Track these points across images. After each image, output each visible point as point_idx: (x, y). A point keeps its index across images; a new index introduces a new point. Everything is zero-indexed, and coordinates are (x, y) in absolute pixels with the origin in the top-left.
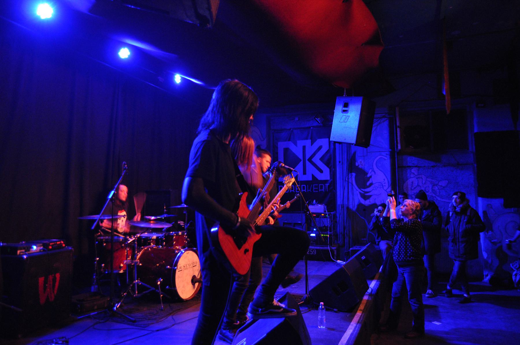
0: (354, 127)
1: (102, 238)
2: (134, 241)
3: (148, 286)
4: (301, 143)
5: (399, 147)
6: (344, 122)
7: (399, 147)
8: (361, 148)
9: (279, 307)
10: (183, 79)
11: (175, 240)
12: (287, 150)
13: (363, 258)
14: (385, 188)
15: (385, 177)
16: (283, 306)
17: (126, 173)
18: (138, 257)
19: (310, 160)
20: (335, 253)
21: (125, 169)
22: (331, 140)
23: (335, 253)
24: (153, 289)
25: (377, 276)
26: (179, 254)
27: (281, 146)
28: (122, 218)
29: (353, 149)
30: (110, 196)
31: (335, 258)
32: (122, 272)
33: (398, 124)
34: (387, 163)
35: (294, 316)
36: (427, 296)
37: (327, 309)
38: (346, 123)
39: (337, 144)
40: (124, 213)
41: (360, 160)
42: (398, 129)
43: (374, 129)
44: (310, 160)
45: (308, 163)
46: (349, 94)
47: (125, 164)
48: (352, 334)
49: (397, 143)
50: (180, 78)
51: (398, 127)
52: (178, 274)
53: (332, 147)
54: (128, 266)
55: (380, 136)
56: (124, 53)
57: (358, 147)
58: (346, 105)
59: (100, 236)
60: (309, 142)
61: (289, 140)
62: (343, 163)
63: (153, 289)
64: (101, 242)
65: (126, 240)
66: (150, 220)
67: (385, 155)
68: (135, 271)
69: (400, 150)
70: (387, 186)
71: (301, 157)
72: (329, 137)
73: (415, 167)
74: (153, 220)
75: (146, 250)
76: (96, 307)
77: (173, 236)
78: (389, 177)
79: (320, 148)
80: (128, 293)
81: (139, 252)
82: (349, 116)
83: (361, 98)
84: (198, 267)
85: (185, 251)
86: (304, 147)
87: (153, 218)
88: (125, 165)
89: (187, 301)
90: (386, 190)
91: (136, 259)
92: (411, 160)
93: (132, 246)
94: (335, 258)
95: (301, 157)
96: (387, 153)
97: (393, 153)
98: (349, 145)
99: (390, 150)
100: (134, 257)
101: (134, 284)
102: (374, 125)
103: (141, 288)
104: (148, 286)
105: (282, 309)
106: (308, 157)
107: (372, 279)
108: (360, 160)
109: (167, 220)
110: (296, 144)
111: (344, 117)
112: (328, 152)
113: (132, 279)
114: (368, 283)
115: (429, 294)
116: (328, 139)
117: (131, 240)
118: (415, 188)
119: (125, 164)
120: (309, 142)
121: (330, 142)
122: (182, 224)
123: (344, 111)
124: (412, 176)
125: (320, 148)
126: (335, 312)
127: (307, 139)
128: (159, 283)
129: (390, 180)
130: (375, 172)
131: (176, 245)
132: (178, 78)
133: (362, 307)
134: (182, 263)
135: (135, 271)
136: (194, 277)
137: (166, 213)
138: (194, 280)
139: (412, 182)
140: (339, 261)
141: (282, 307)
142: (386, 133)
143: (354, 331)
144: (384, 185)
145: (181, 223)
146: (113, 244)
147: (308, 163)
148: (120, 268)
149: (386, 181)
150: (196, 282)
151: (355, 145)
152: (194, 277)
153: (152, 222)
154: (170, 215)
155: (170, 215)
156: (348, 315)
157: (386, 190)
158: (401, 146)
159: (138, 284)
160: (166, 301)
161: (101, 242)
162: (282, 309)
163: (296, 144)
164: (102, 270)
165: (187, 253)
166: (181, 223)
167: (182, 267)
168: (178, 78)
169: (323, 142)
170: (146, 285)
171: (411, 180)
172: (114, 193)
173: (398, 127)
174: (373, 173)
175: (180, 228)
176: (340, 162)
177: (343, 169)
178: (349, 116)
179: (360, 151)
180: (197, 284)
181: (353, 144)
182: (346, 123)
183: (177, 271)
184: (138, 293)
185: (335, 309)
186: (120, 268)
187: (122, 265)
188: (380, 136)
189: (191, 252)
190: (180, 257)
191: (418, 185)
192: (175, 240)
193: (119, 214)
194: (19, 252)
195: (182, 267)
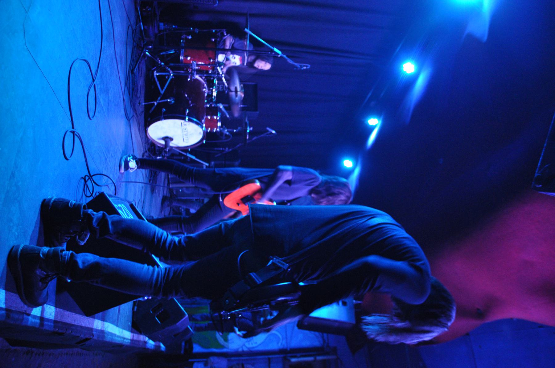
5: (294, 360)
11: (212, 118)
14: (247, 344)
15: (258, 343)
24: (162, 92)
30: (276, 50)
32: (181, 58)
33: (319, 358)
47: (307, 66)
51: (315, 358)
52: (178, 122)
54: (188, 65)
69: (289, 361)
75: (203, 85)
78: (261, 348)
84: (182, 144)
89: (146, 131)
96: (285, 346)
99: (288, 349)
100: (199, 72)
129: (256, 349)
136: (172, 139)
138: (167, 139)
142: (306, 344)
143: (118, 337)
144: (250, 343)
146: (209, 46)
148: (186, 56)
149: (254, 345)
150: (166, 142)
152: (172, 139)
160: (147, 108)
164: (184, 36)
165: (200, 133)
172: (278, 54)
180: (163, 142)
185: (136, 308)
187: (189, 58)
189: (200, 137)
192: (212, 118)
195: (185, 127)
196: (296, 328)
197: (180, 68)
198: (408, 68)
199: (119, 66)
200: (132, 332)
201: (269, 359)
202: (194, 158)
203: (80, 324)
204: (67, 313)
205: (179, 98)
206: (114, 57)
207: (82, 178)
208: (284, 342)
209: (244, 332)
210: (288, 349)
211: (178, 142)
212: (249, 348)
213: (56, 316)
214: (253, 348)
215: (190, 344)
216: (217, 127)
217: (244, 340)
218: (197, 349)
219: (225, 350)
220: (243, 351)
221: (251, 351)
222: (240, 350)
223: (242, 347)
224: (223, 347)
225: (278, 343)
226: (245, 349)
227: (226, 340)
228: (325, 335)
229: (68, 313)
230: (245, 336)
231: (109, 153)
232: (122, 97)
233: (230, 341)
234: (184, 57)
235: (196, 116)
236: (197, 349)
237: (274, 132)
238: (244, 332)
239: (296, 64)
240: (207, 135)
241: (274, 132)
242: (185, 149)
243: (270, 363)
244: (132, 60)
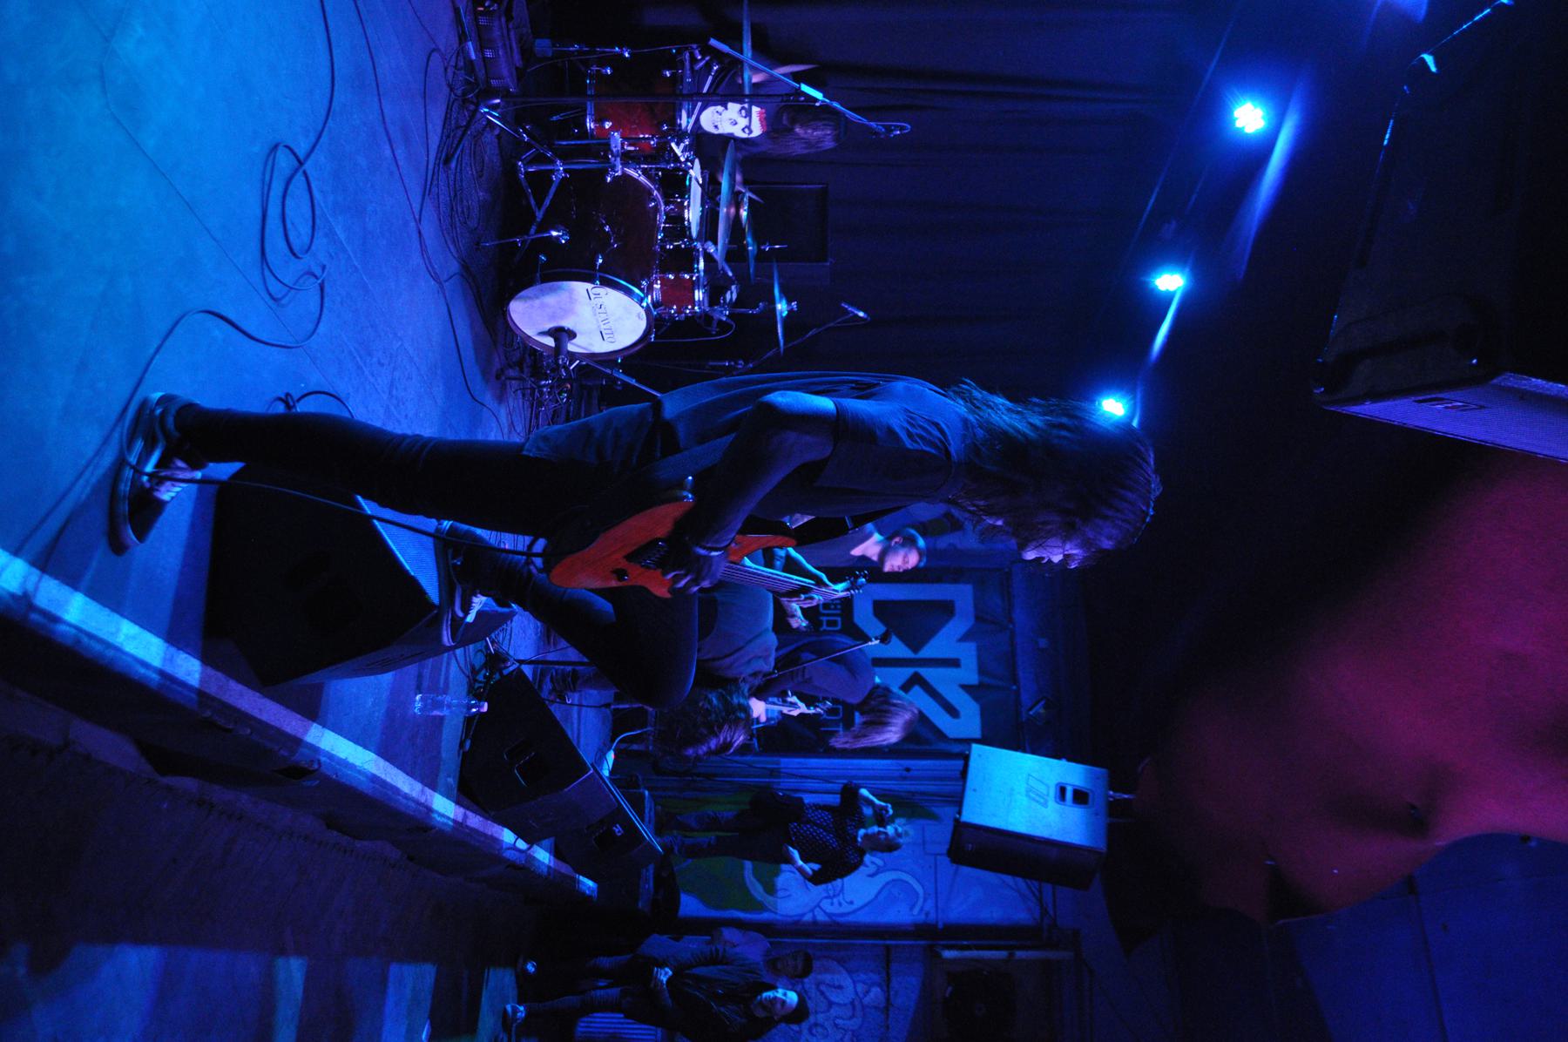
0: (1011, 820)
1: (687, 64)
2: (676, 158)
3: (547, 202)
4: (968, 653)
5: (948, 954)
6: (1029, 790)
7: (948, 954)
8: (948, 837)
9: (466, 609)
10: (1169, 298)
12: (945, 610)
13: (618, 829)
14: (826, 905)
16: (470, 619)
17: (877, 134)
18: (631, 172)
19: (916, 680)
20: (635, 747)
21: (889, 129)
22: (975, 747)
23: (635, 747)
24: (540, 214)
25: (565, 869)
26: (637, 291)
27: (962, 594)
28: (743, 122)
29: (948, 811)
31: (623, 746)
32: (590, 125)
33: (1019, 954)
34: (900, 914)
35: (439, 637)
36: (509, 1008)
37: (469, 720)
38: (1024, 792)
39: (960, 763)
40: (757, 130)
41: (911, 832)
42: (1003, 954)
43: (1009, 879)
44: (916, 680)
45: (908, 672)
46: (1114, 808)
47: (902, 128)
48: (396, 790)
49: (962, 948)
50: (1172, 289)
51: (1011, 955)
53: (956, 749)
55: (983, 898)
56: (1249, 116)
57: (950, 828)
58: (1080, 797)
59: (693, 60)
60: (973, 678)
61: (978, 618)
62: (904, 778)
63: (540, 214)
64: (674, 63)
65: (680, 135)
66: (738, 207)
67: (927, 908)
68: (592, 164)
70: (829, 909)
71: (927, 652)
72: (984, 741)
73: (888, 999)
74: (738, 215)
76: (489, 54)
77: (691, 271)
78: (864, 918)
79: (953, 711)
80: (529, 146)
81: (645, 172)
82: (1045, 805)
83: (1102, 845)
85: (648, 310)
86: (954, 663)
87: (744, 214)
88: (900, 129)
89: (505, 313)
90: (818, 906)
91: (625, 164)
92: (908, 987)
93: (663, 152)
94: (623, 746)
95: (927, 652)
96: (932, 916)
97: (931, 935)
98: (958, 800)
99: (940, 926)
100: (627, 158)
101: (553, 162)
102: (1020, 881)
103: (541, 181)
104: (547, 202)
105: (461, 614)
106: (925, 672)
107: (557, 853)
108: (911, 832)
109: (735, 254)
110: (965, 638)
111: (1043, 789)
112: (941, 735)
113: (566, 155)
114: (546, 842)
115: (515, 1011)
116: (977, 734)
117: (678, 151)
118: (822, 993)
119: (902, 128)
120: (973, 678)
121: (969, 741)
122: (728, 296)
123: (1062, 790)
124: (860, 987)
125: (953, 711)
126: (462, 745)
127: (982, 670)
128: (554, 234)
129: (850, 918)
130: (872, 876)
131: (665, 282)
132: (1170, 282)
133: (475, 821)
134: (612, 298)
135: (592, 164)
136: (572, 335)
137: (760, 252)
139: (840, 987)
140: (611, 756)
141: (466, 613)
142: (992, 914)
143: (406, 796)
145: (732, 295)
147: (908, 672)
149: (846, 908)
151: (957, 821)
152: (572, 335)
153: (733, 210)
154: (752, 263)
155: (752, 263)
156: (450, 780)
157: (818, 906)
158: (954, 961)
159: (552, 172)
161: (674, 63)
162: (461, 614)
163: (965, 638)
166: (732, 295)
167: (599, 301)
168: (1170, 282)
169: (969, 721)
170: (550, 196)
171: (847, 982)
172: (816, 100)
173: (1011, 955)
174: (872, 869)
175: (715, 295)
176: (908, 770)
177: (882, 778)
178: (1045, 805)
179: (940, 834)
180: (550, 341)
181: (960, 813)
182: (1024, 792)
183: (589, 286)
184: (527, 173)
185: (468, 743)
186: (599, 120)
188: (983, 898)
189: (643, 325)
190: (629, 293)
191: (831, 1004)
193: (755, 110)
194: (485, 708)
195: (599, 301)
196: (945, 861)
197: (586, 152)
198: (1249, 116)
199: (399, 152)
200: (458, 803)
201: (888, 948)
202: (633, 382)
203: (277, 724)
204: (233, 684)
205: (582, 232)
206: (381, 130)
207: (280, 399)
208: (929, 905)
209: (816, 867)
210: (940, 926)
211: (589, 341)
212: (829, 915)
213: (202, 681)
214: (842, 915)
215: (668, 890)
216: (693, 302)
217: (818, 891)
218: (690, 905)
219: (765, 916)
220: (815, 922)
221: (838, 924)
222: (808, 918)
223: (812, 910)
224: (762, 907)
225: (911, 909)
226: (821, 917)
227: (771, 889)
228: (1047, 888)
229: (240, 687)
230: (816, 879)
231: (370, 355)
232: (413, 224)
233: (780, 894)
234: (595, 121)
235: (619, 271)
236: (690, 905)
237: (861, 314)
238: (816, 867)
239: (873, 124)
240: (656, 323)
241: (861, 314)
242: (607, 359)
243: (888, 962)
244: (445, 137)
